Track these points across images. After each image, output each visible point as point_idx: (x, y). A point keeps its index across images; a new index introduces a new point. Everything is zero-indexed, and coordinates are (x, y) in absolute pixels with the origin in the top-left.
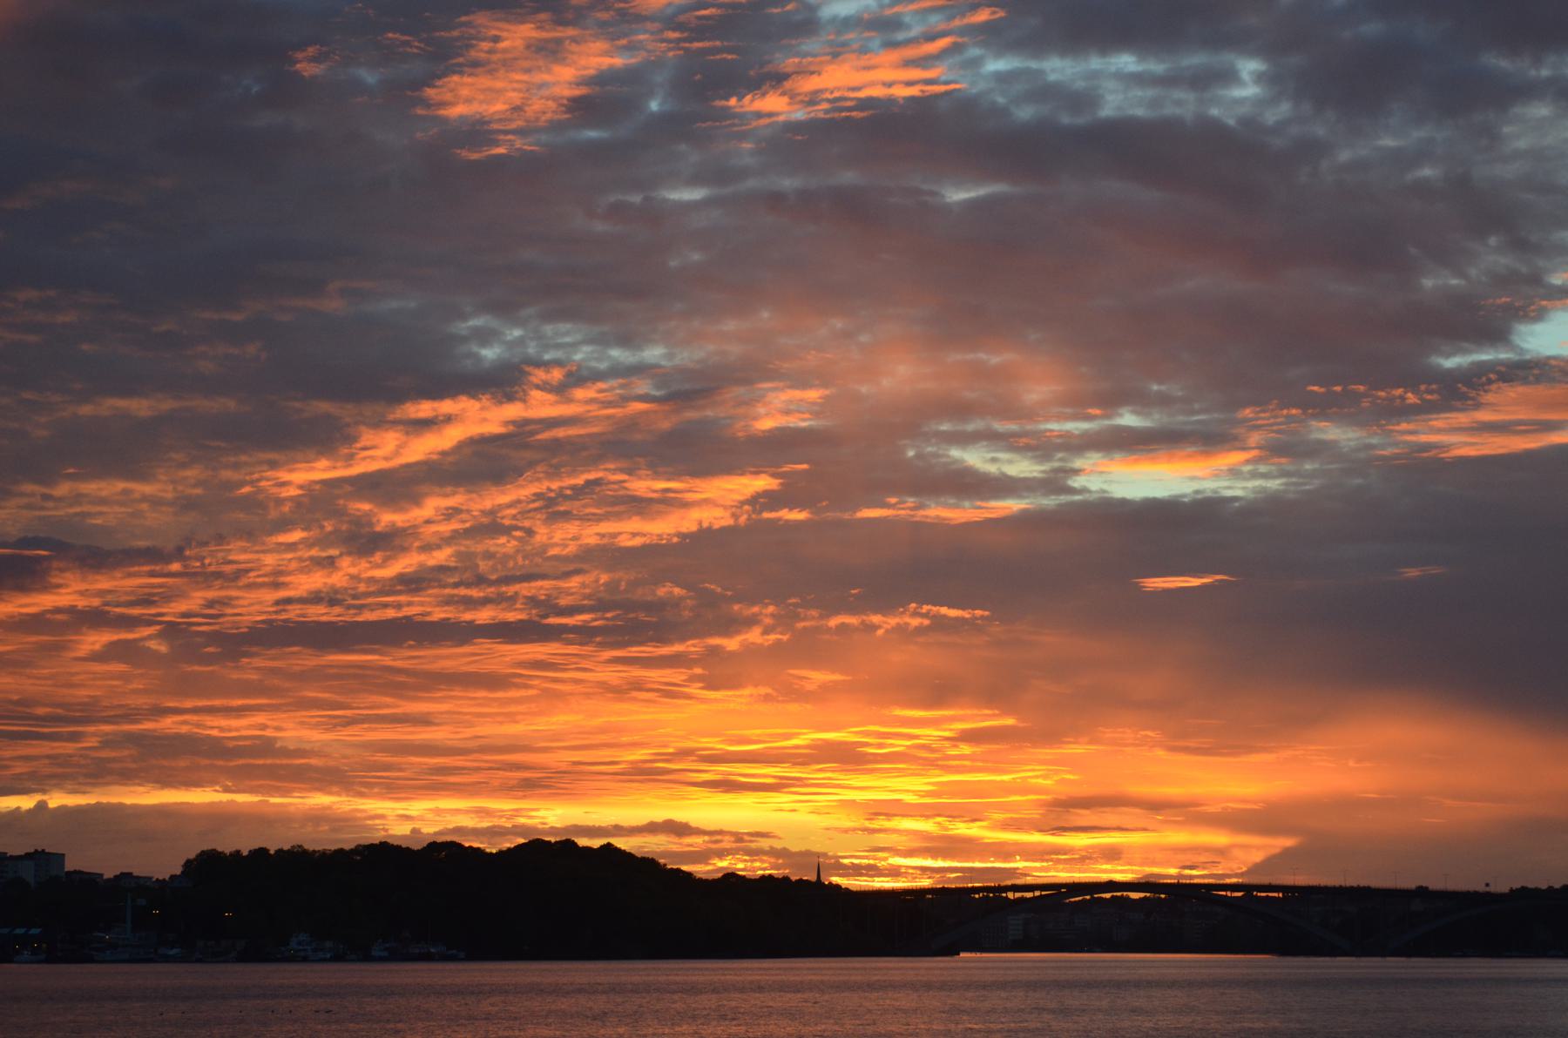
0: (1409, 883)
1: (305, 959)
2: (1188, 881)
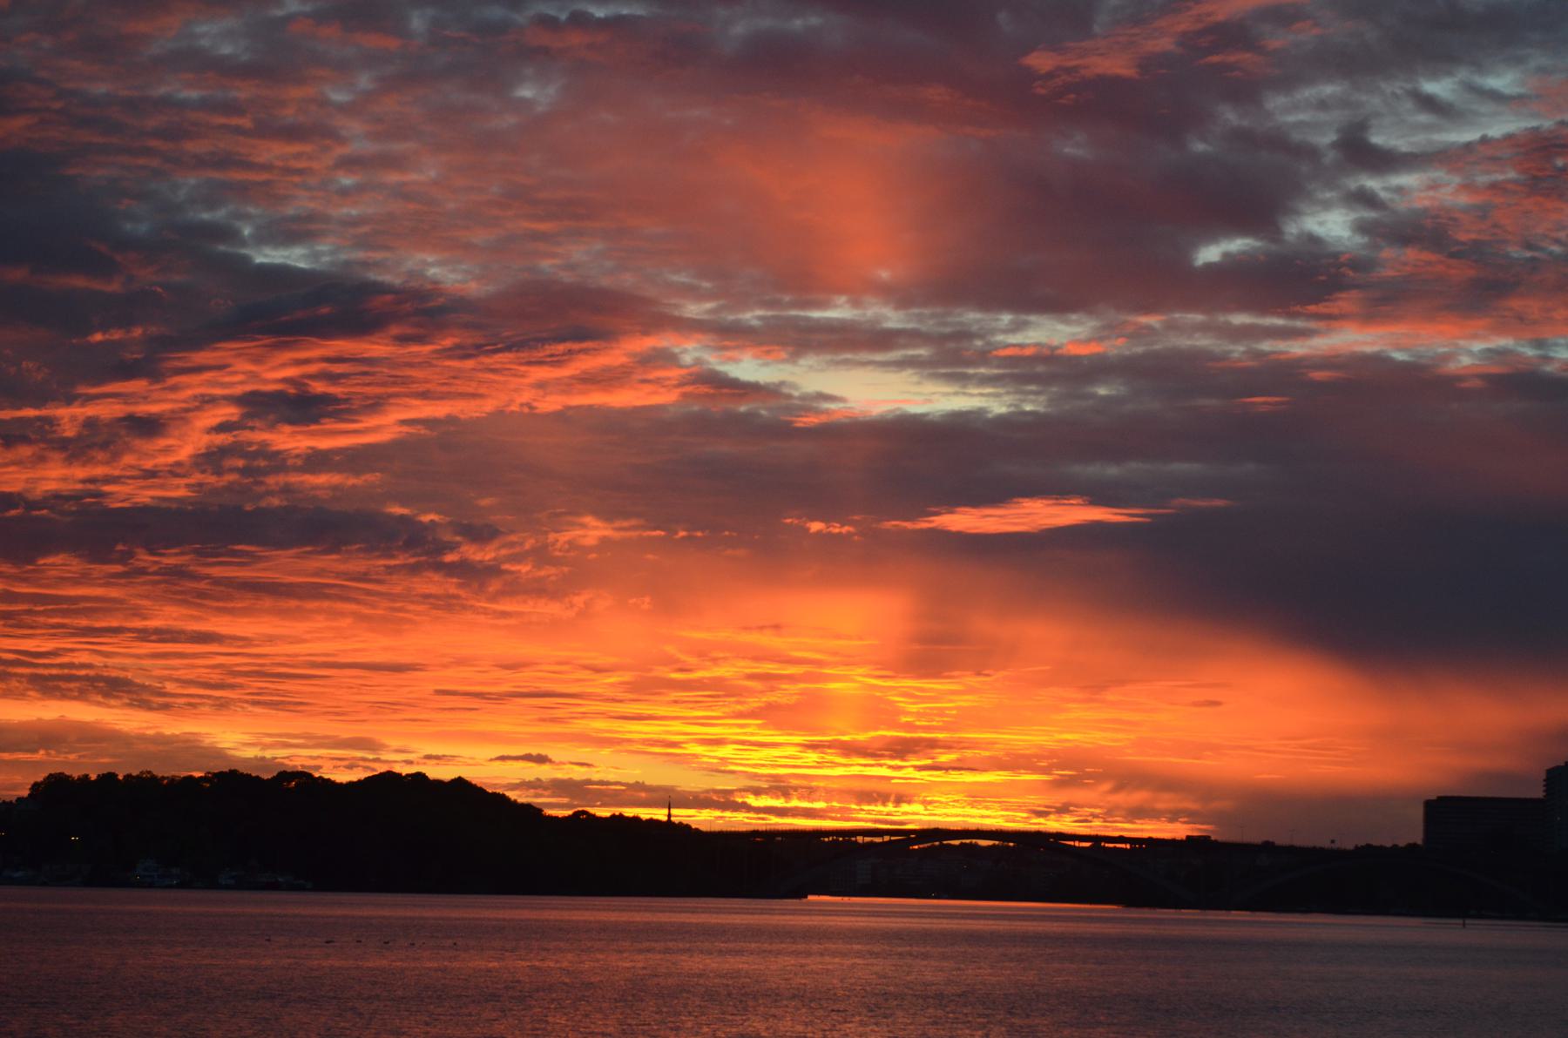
0: (1254, 836)
1: (151, 886)
2: (660, 814)
